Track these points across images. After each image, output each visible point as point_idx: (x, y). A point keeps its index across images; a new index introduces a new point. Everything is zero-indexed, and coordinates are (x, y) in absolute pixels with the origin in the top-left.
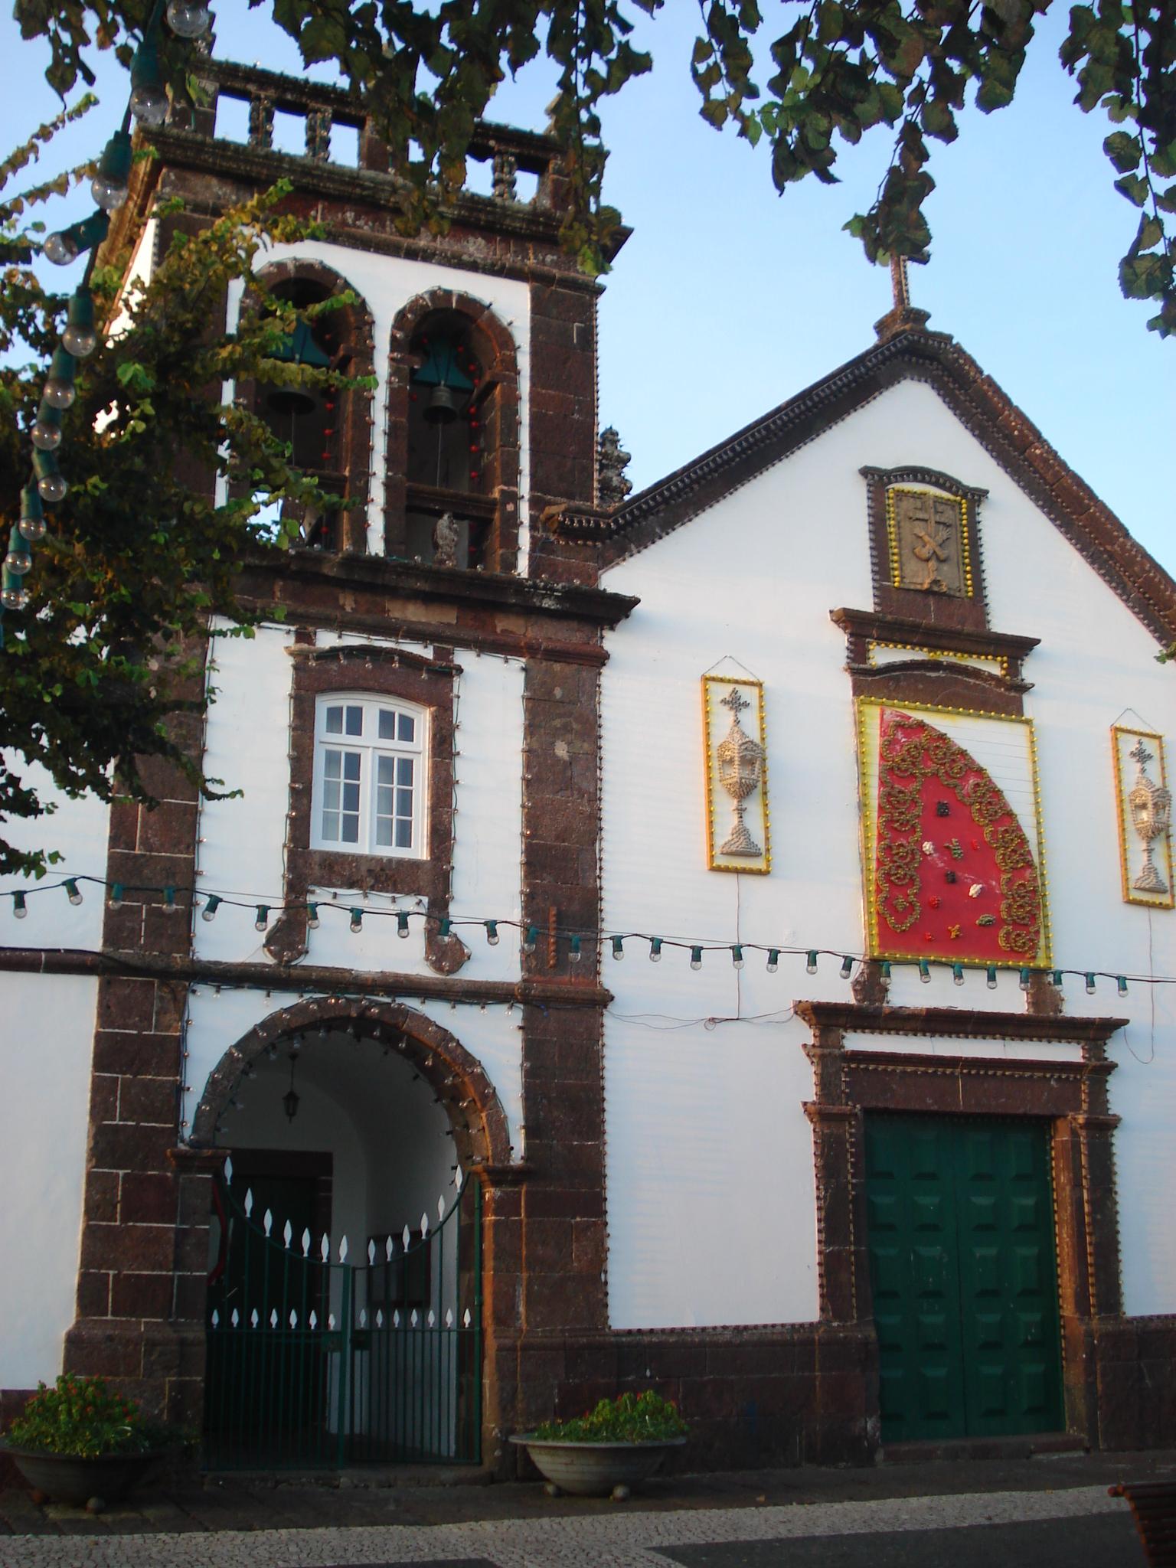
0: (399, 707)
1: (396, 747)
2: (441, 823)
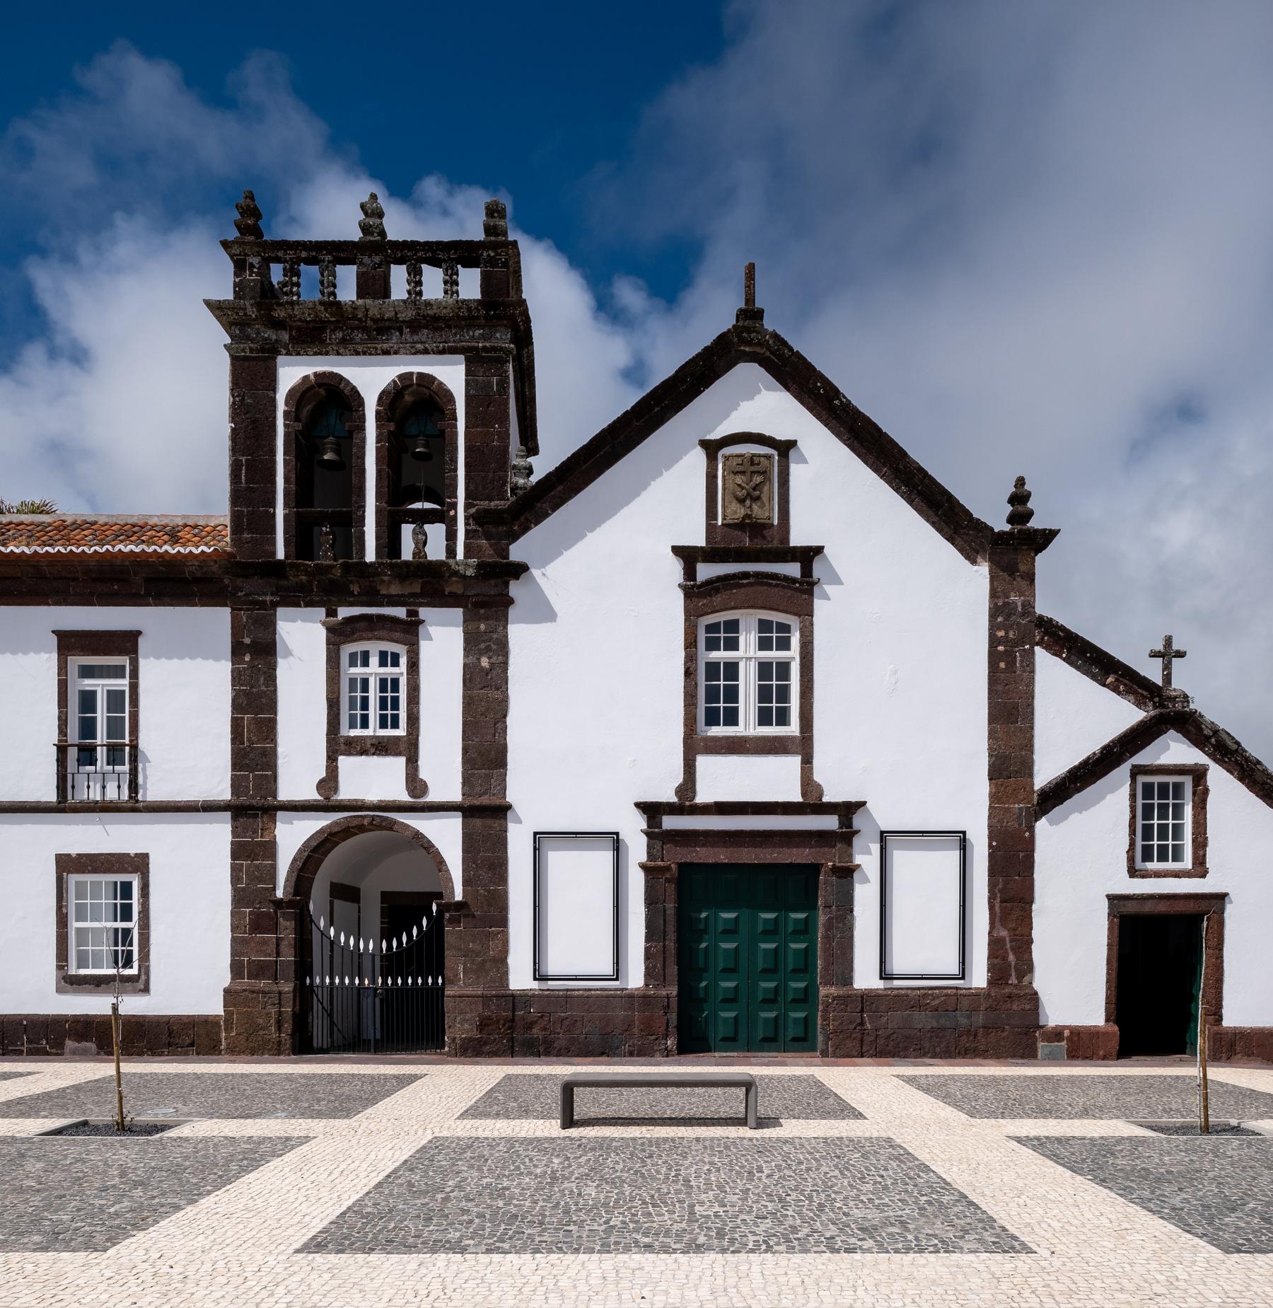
1: (389, 671)
2: (413, 713)
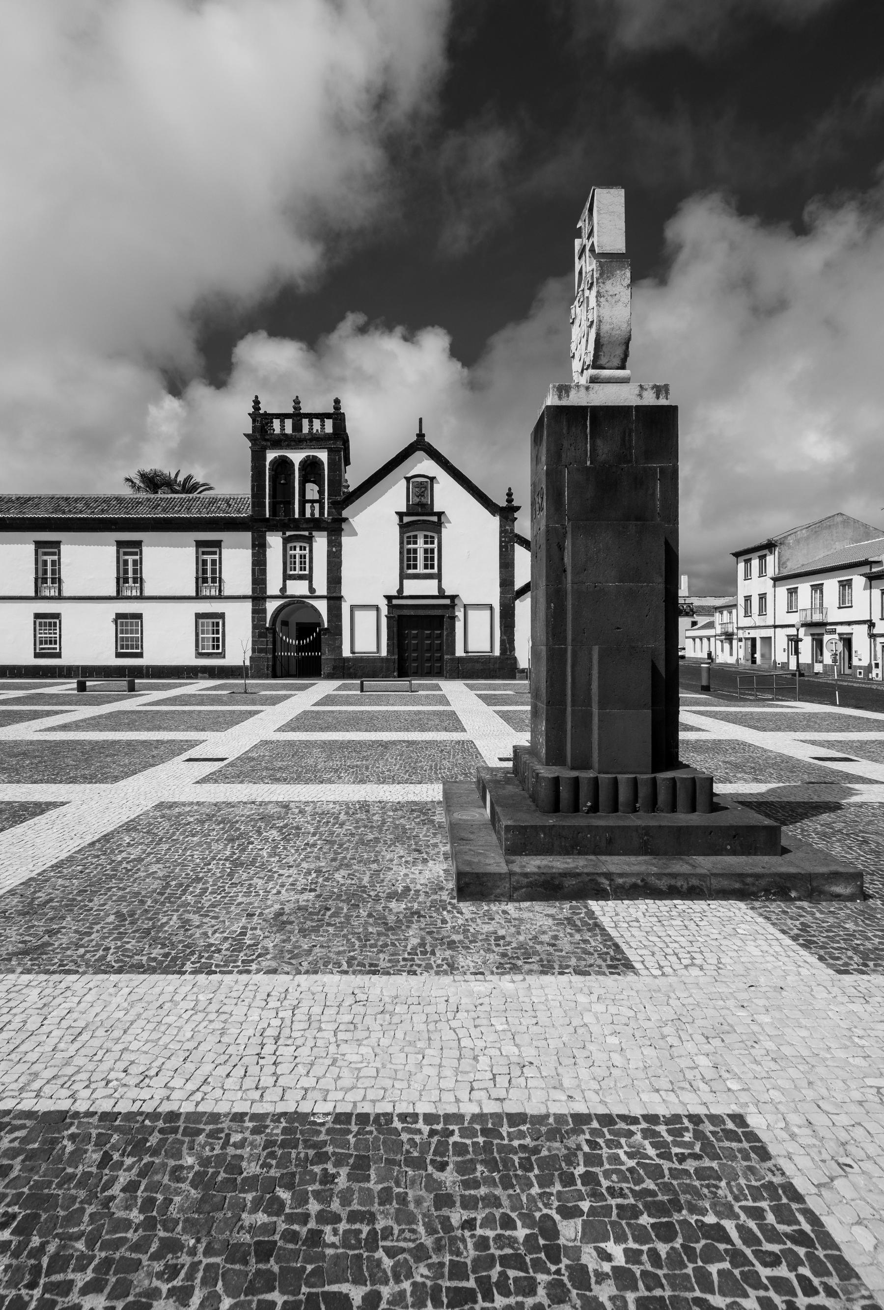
0: (303, 544)
